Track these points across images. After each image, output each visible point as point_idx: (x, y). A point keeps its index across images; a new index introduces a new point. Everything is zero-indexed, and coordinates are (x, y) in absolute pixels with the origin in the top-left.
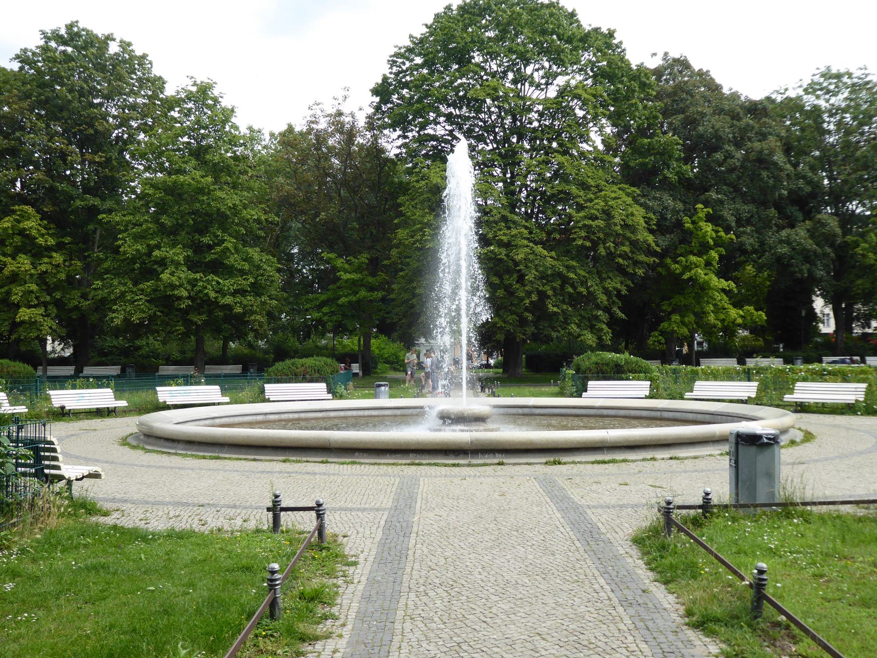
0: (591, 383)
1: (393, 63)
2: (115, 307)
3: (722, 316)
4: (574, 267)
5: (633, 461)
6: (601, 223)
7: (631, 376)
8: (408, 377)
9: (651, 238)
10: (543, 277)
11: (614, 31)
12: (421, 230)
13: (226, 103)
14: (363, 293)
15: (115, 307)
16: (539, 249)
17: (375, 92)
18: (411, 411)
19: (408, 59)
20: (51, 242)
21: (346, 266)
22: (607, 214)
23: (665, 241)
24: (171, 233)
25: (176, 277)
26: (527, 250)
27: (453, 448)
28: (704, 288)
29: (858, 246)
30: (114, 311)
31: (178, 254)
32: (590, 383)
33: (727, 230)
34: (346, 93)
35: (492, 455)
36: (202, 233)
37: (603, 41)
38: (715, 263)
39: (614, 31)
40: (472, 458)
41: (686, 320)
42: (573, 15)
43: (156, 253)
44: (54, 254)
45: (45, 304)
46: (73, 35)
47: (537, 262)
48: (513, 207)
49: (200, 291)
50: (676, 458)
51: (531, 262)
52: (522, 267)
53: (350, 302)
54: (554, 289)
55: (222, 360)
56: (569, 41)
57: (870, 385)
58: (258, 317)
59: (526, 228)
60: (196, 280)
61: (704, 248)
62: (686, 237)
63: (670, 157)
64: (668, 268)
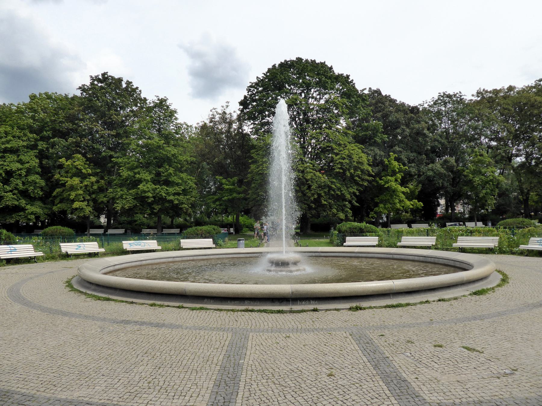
0: (348, 238)
1: (249, 90)
2: (117, 202)
3: (403, 205)
4: (334, 182)
5: (415, 304)
6: (347, 161)
7: (368, 234)
8: (256, 235)
9: (370, 169)
10: (320, 186)
11: (349, 76)
12: (262, 165)
13: (172, 108)
14: (235, 195)
15: (117, 202)
16: (318, 174)
17: (241, 103)
18: (255, 255)
19: (256, 88)
20: (90, 171)
21: (227, 183)
22: (350, 157)
23: (376, 169)
24: (146, 166)
25: (147, 188)
26: (312, 174)
27: (278, 297)
28: (394, 191)
29: (464, 171)
30: (117, 203)
31: (146, 176)
32: (347, 238)
33: (404, 165)
34: (227, 104)
35: (307, 302)
36: (159, 167)
37: (345, 80)
38: (399, 180)
39: (349, 76)
40: (293, 304)
41: (387, 206)
42: (331, 68)
43: (137, 176)
44: (91, 177)
45: (88, 201)
46: (105, 78)
47: (316, 180)
48: (305, 153)
49: (158, 193)
50: (443, 300)
51: (314, 179)
52: (310, 182)
53: (229, 199)
54: (325, 192)
55: (171, 227)
56: (330, 78)
57: (500, 238)
58: (186, 206)
59: (311, 164)
60: (156, 189)
61: (394, 173)
62: (385, 168)
63: (377, 131)
64: (377, 182)
